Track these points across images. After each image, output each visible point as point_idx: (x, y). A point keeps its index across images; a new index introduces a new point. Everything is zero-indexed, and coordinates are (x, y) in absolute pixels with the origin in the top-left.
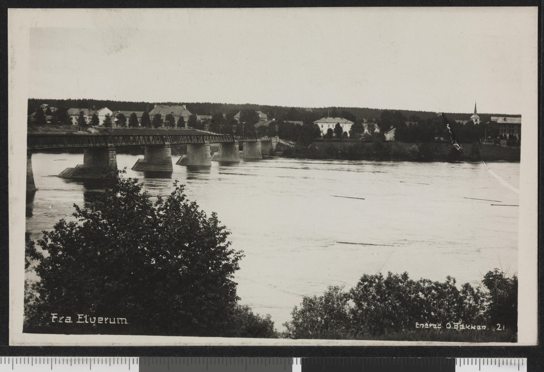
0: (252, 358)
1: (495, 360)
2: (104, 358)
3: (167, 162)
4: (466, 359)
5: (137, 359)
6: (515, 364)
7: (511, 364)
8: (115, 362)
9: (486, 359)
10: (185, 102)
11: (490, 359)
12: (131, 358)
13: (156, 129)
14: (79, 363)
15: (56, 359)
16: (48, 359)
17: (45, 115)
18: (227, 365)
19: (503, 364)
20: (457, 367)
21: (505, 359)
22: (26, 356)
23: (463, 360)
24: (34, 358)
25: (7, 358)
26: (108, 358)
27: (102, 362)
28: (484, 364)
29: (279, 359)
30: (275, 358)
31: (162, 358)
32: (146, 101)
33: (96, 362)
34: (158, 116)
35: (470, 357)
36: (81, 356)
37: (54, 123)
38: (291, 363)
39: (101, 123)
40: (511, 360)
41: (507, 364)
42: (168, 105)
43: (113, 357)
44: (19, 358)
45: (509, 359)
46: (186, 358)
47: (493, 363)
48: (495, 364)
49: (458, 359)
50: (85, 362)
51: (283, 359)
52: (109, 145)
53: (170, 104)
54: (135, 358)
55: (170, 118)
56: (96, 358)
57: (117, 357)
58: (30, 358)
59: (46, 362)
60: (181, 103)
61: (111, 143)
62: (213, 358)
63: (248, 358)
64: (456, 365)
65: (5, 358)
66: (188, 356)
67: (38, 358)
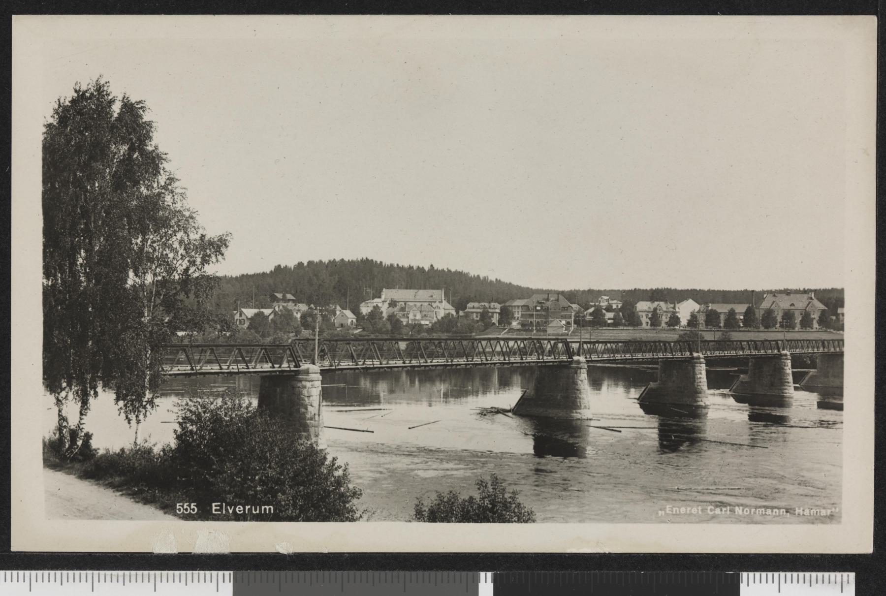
0: (414, 573)
1: (804, 575)
2: (121, 573)
3: (786, 382)
4: (757, 574)
5: (230, 574)
6: (836, 583)
7: (829, 583)
8: (175, 580)
9: (789, 574)
10: (813, 288)
11: (795, 574)
12: (221, 573)
13: (711, 307)
14: (136, 582)
15: (143, 575)
16: (149, 574)
17: (604, 311)
18: (373, 584)
19: (817, 583)
20: (743, 586)
21: (820, 574)
22: (52, 569)
23: (797, 576)
24: (65, 572)
25: (21, 572)
26: (183, 573)
27: (174, 579)
28: (786, 583)
29: (458, 573)
30: (452, 573)
31: (271, 573)
32: (750, 289)
33: (165, 579)
34: (769, 313)
35: (751, 571)
36: (116, 570)
37: (616, 323)
38: (477, 581)
39: (684, 322)
40: (829, 576)
41: (823, 583)
42: (785, 293)
43: (191, 572)
44: (40, 572)
45: (826, 574)
46: (308, 573)
47: (801, 580)
48: (804, 583)
49: (744, 575)
50: (146, 579)
51: (464, 573)
52: (695, 355)
53: (787, 292)
54: (227, 573)
55: (788, 316)
56: (164, 573)
57: (197, 572)
58: (58, 572)
59: (177, 579)
60: (806, 289)
61: (698, 352)
62: (352, 573)
63: (408, 573)
64: (741, 584)
65: (18, 573)
66: (312, 569)
67: (71, 573)
